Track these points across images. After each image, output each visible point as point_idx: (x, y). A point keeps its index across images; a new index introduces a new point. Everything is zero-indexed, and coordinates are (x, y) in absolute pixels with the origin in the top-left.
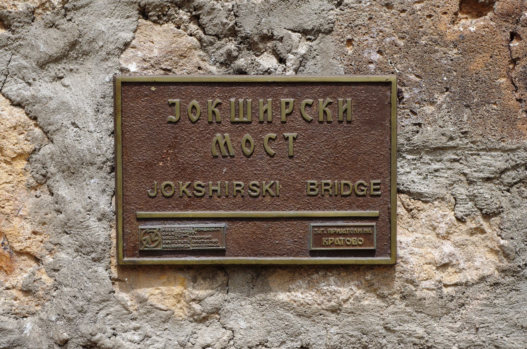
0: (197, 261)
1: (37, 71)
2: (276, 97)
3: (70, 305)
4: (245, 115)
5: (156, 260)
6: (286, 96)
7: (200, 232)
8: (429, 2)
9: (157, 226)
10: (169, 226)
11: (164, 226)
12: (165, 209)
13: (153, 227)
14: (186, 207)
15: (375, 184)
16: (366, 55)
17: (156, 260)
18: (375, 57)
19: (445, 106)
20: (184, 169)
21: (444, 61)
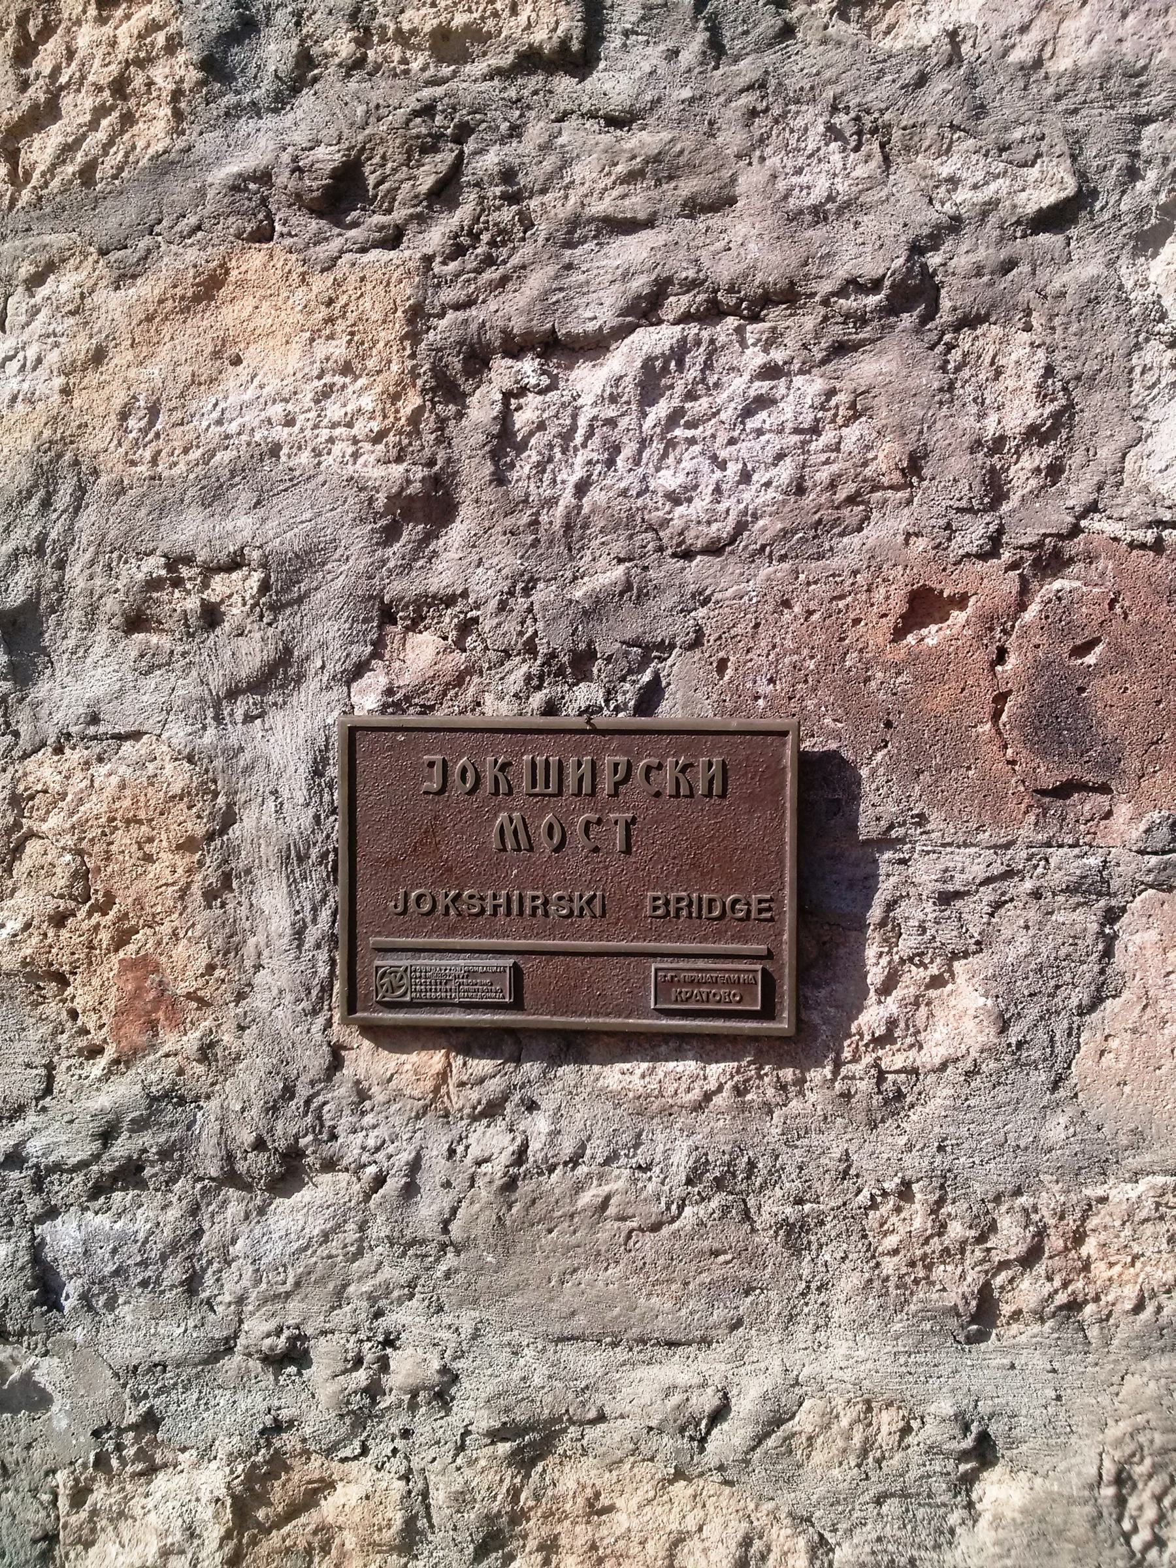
0: (469, 1021)
1: (291, 379)
2: (601, 751)
3: (559, 479)
4: (547, 787)
5: (401, 1016)
6: (615, 752)
7: (470, 973)
8: (5, 1539)
9: (404, 961)
10: (423, 961)
11: (414, 962)
12: (417, 934)
13: (397, 963)
14: (452, 931)
15: (760, 901)
16: (749, 685)
17: (401, 1016)
18: (764, 688)
19: (881, 771)
20: (450, 870)
21: (881, 696)
